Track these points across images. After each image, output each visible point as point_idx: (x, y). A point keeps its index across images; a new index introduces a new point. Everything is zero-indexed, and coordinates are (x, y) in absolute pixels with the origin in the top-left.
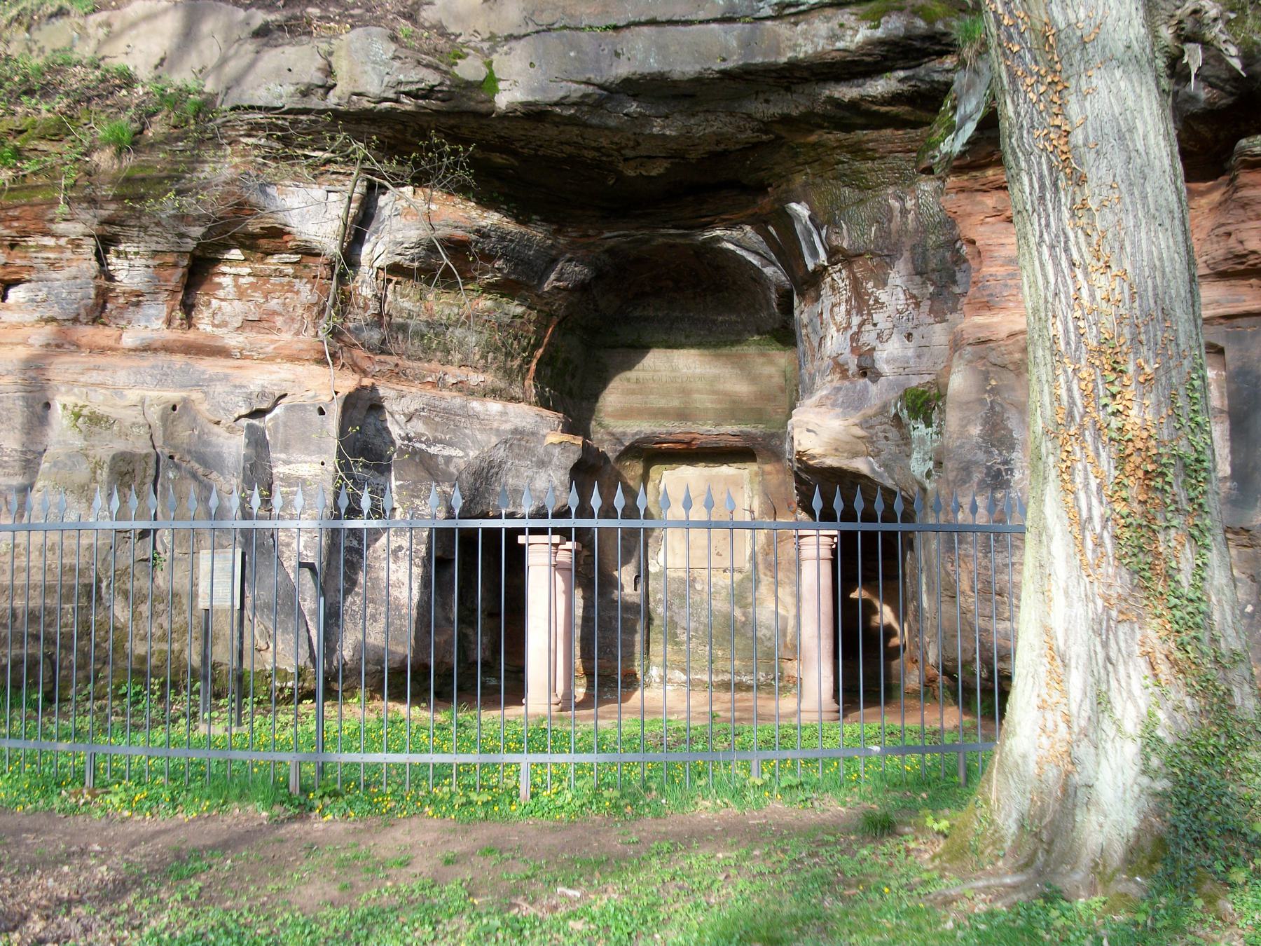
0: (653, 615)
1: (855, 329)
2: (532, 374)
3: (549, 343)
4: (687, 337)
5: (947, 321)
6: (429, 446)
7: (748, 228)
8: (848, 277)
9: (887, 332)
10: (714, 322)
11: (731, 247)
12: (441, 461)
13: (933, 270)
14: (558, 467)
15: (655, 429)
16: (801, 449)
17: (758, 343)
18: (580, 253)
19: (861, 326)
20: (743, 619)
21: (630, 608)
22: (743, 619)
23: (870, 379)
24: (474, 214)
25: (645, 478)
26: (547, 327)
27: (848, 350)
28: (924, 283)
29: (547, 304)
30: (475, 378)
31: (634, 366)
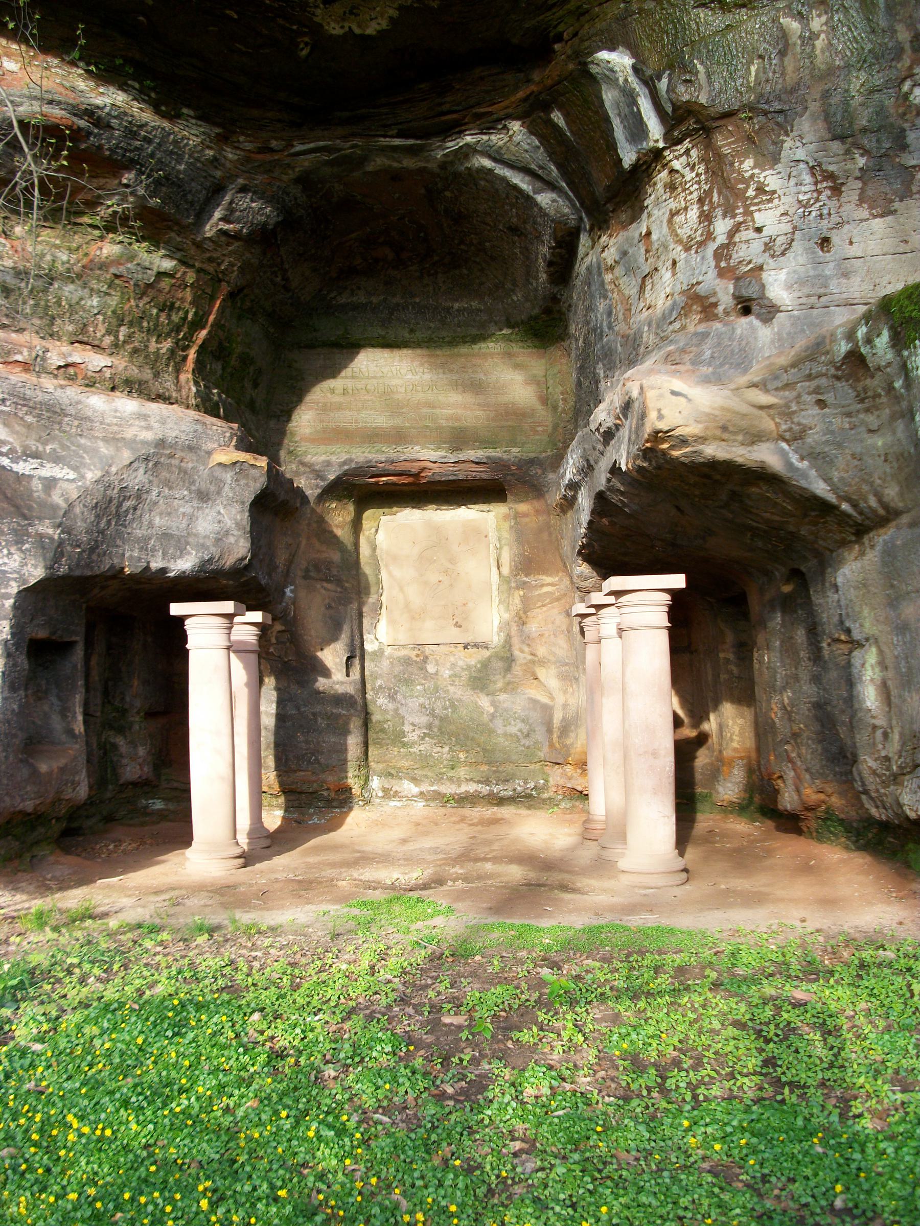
0: (371, 708)
1: (721, 239)
2: (190, 364)
3: (216, 324)
4: (412, 331)
5: (893, 212)
6: (15, 461)
7: (516, 126)
8: (702, 160)
9: (781, 240)
10: (448, 310)
11: (487, 163)
12: (36, 485)
13: (864, 130)
14: (231, 501)
15: (370, 456)
16: (662, 426)
17: (508, 339)
18: (260, 179)
19: (731, 234)
20: (492, 710)
21: (340, 700)
22: (492, 710)
23: (758, 316)
24: (81, 85)
25: (357, 525)
26: (212, 298)
27: (712, 274)
28: (848, 152)
29: (210, 260)
30: (96, 361)
31: (339, 372)
